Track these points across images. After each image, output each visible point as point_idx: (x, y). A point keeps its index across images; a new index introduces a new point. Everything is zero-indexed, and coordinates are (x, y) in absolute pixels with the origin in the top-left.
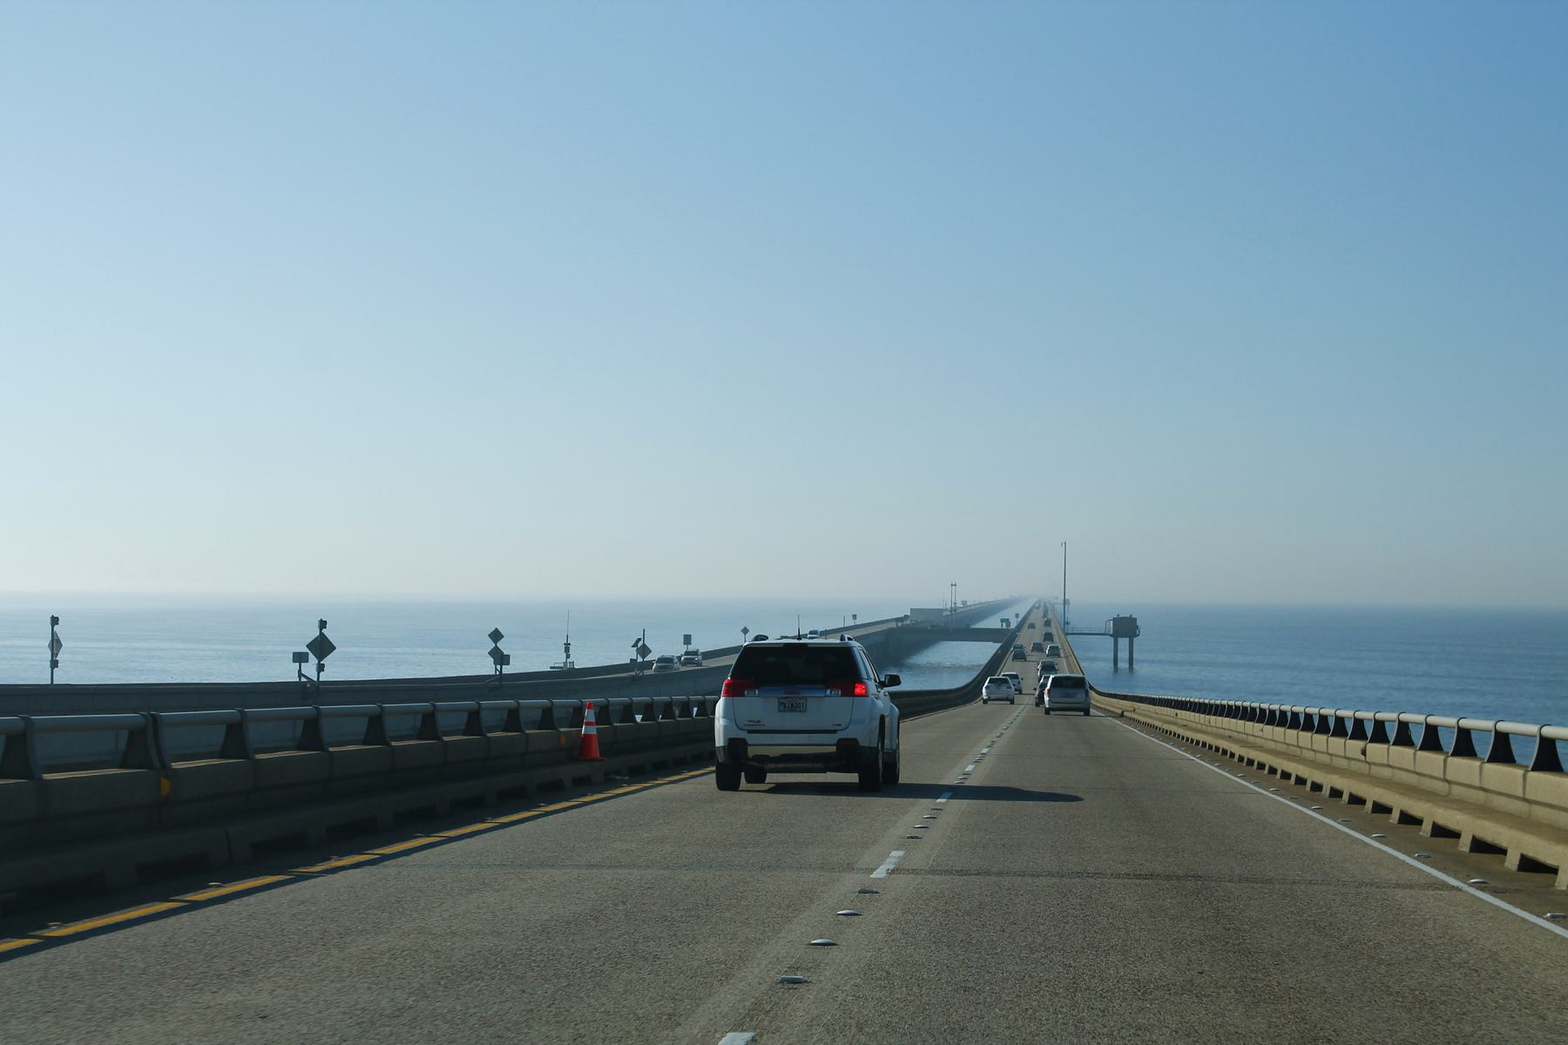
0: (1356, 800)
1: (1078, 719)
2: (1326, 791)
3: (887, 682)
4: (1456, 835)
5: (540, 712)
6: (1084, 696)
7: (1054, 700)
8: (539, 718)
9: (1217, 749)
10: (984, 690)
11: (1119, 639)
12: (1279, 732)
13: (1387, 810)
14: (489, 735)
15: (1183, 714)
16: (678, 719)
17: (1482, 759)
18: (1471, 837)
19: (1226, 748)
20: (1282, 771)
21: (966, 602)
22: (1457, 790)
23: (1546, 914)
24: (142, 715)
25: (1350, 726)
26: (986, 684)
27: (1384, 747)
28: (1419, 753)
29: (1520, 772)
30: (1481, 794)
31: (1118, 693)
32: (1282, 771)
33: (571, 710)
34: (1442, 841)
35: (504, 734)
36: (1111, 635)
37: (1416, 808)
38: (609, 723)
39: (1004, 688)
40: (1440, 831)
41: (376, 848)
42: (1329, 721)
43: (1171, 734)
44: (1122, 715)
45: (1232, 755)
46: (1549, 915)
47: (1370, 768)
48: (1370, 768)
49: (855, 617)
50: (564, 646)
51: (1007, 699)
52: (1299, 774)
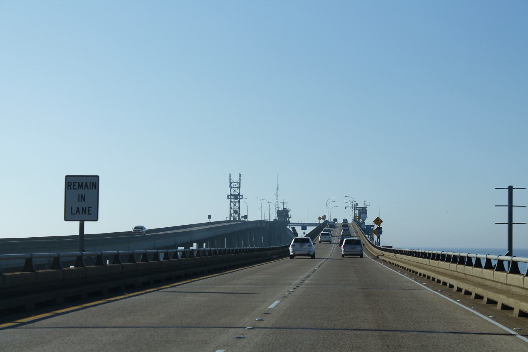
0: (468, 293)
1: (358, 259)
2: (455, 288)
4: (512, 309)
5: (24, 261)
6: (360, 248)
7: (346, 250)
8: (24, 265)
9: (410, 270)
10: (290, 248)
12: (454, 266)
13: (495, 303)
14: (86, 267)
16: (196, 258)
17: (523, 275)
18: (501, 304)
19: (414, 270)
20: (450, 284)
22: (468, 277)
23: (514, 329)
25: (474, 261)
26: (292, 243)
27: (480, 269)
28: (484, 270)
29: (522, 277)
32: (450, 284)
33: (52, 259)
34: (479, 301)
35: (129, 263)
37: (511, 302)
38: (169, 259)
39: (306, 246)
40: (505, 307)
41: (53, 311)
42: (473, 260)
43: (394, 264)
44: (378, 257)
45: (417, 273)
46: (515, 329)
47: (466, 276)
48: (466, 276)
51: (308, 255)
52: (428, 275)
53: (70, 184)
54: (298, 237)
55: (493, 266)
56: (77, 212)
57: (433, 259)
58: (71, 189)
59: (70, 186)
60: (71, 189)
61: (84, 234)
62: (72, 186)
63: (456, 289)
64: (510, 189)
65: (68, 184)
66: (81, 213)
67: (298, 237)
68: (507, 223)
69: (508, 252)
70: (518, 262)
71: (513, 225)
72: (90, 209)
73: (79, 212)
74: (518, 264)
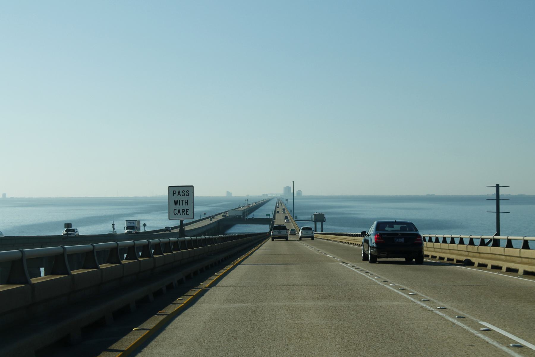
3: (395, 239)
11: (317, 223)
15: (322, 235)
21: (188, 191)
24: (62, 247)
27: (439, 244)
30: (449, 251)
31: (496, 330)
36: (314, 221)
49: (205, 214)
50: (112, 225)
53: (183, 211)
54: (71, 227)
55: (486, 243)
56: (178, 213)
57: (356, 236)
58: (184, 214)
59: (184, 212)
60: (184, 214)
61: (317, 222)
62: (185, 212)
63: (456, 261)
64: (498, 186)
65: (182, 210)
66: (181, 214)
67: (71, 227)
68: (495, 212)
69: (497, 232)
70: (485, 239)
71: (500, 213)
72: (188, 210)
73: (180, 213)
74: (439, 239)
